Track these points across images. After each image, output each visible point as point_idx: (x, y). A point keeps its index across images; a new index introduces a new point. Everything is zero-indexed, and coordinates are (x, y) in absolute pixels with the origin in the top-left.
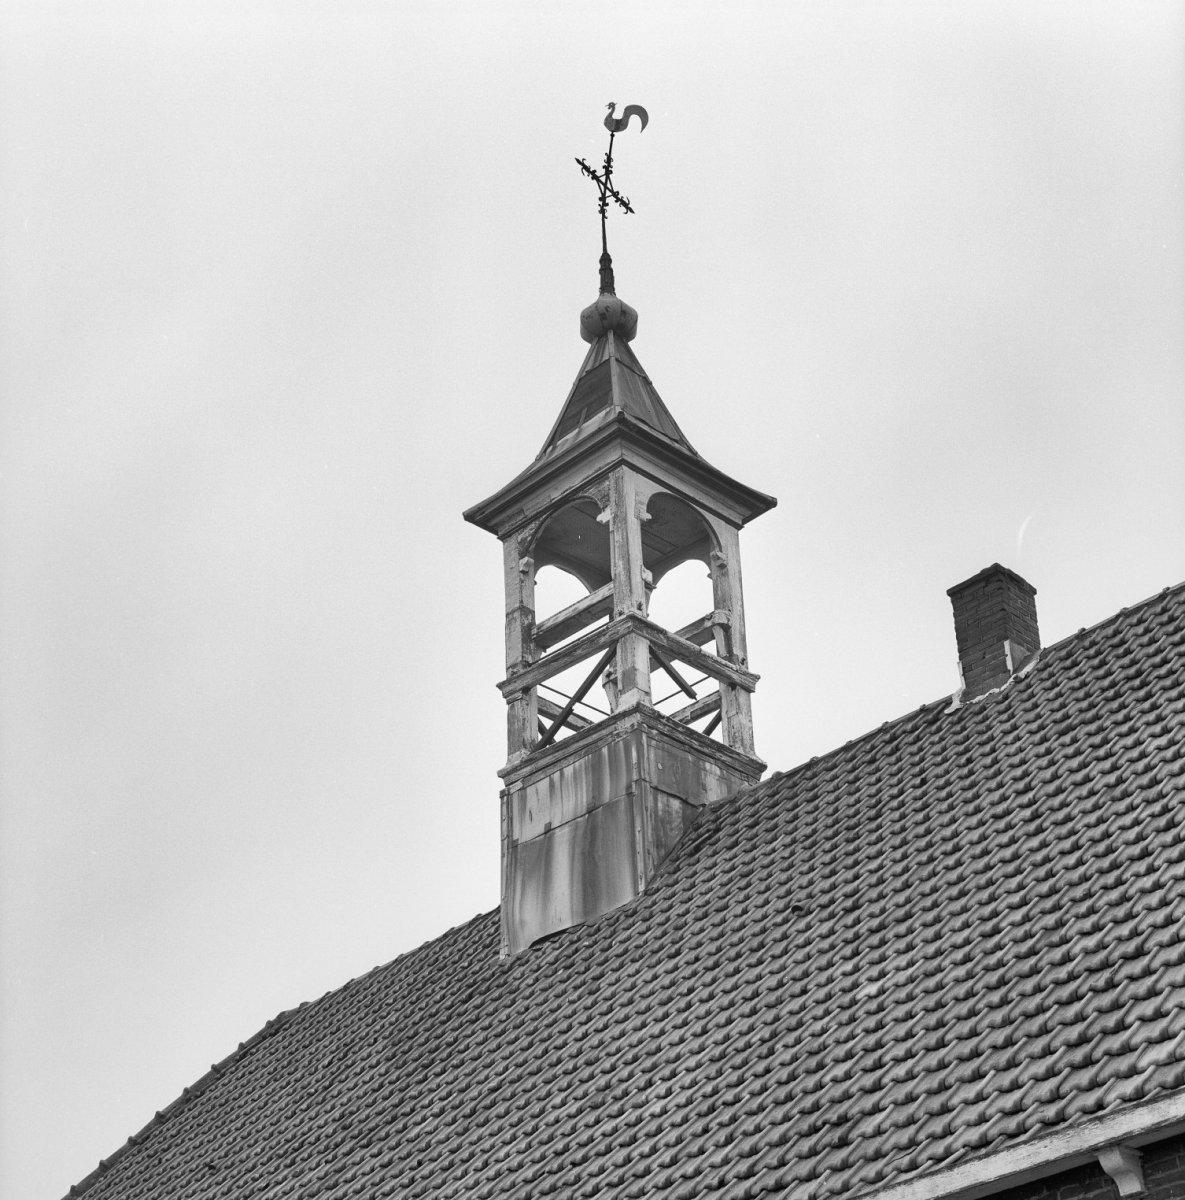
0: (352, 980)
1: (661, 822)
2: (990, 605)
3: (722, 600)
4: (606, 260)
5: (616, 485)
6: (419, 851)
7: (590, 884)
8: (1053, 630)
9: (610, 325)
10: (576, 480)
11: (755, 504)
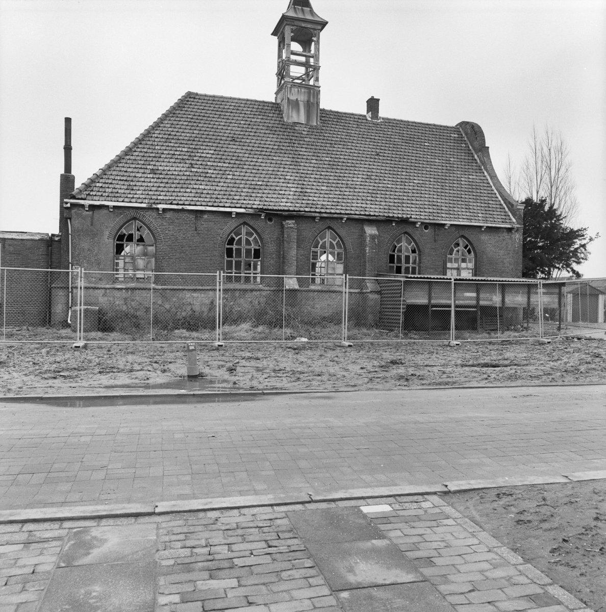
2: (373, 104)
10: (309, 26)
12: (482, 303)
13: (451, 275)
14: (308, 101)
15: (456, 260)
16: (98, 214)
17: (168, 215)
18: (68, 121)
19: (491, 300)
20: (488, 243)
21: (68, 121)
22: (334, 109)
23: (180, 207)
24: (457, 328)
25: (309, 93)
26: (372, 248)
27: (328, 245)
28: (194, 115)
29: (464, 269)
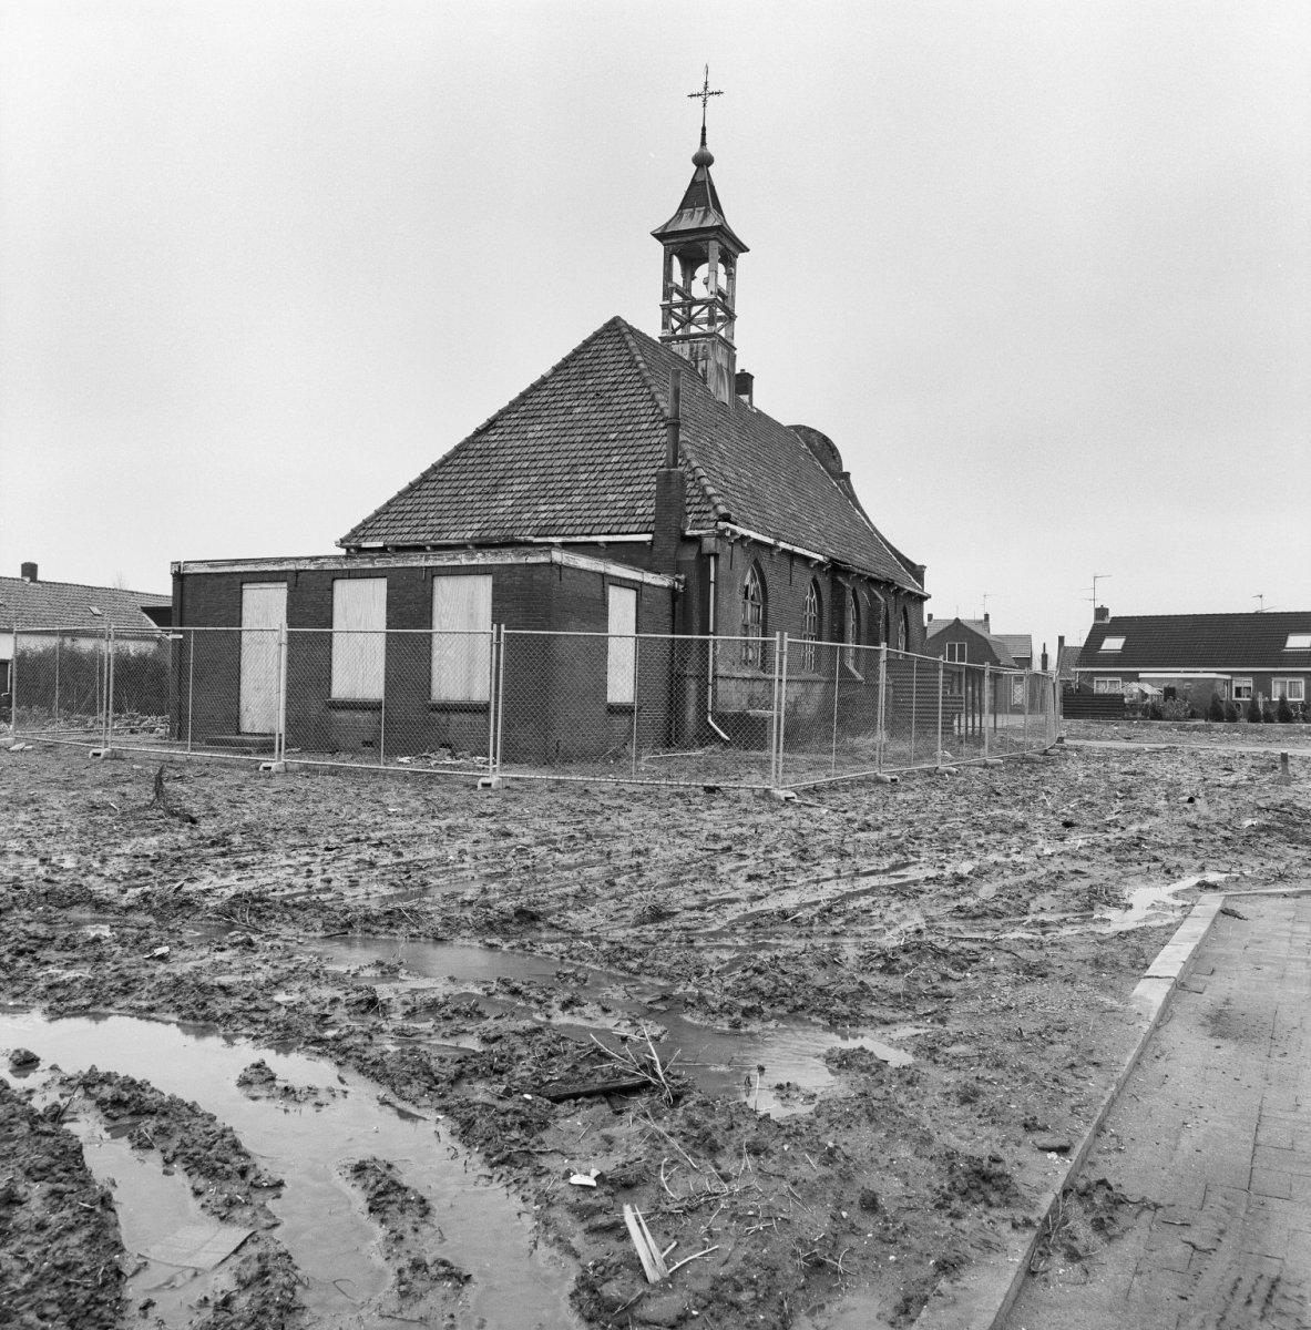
4: (704, 129)
9: (703, 161)
11: (744, 249)
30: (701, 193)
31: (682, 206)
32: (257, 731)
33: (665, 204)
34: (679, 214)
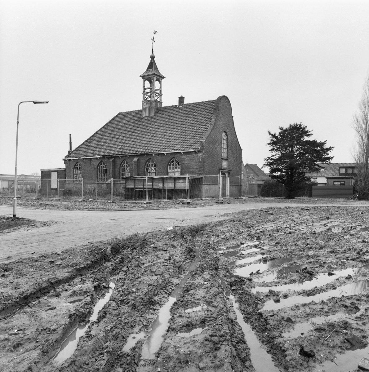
0: (136, 235)
1: (155, 109)
2: (181, 99)
3: (161, 87)
4: (153, 49)
5: (152, 74)
6: (134, 102)
7: (149, 113)
8: (185, 103)
9: (153, 57)
10: (150, 77)
11: (164, 78)
12: (155, 187)
13: (171, 175)
14: (150, 107)
15: (173, 169)
16: (71, 162)
17: (84, 161)
18: (70, 135)
19: (158, 186)
20: (186, 159)
21: (70, 135)
22: (197, 102)
23: (85, 158)
24: (130, 198)
25: (150, 103)
26: (135, 166)
27: (151, 165)
28: (122, 122)
29: (177, 172)
30: (152, 65)
31: (148, 68)
32: (13, 210)
33: (143, 68)
34: (147, 71)
